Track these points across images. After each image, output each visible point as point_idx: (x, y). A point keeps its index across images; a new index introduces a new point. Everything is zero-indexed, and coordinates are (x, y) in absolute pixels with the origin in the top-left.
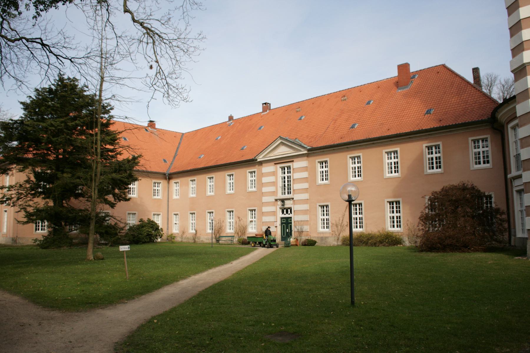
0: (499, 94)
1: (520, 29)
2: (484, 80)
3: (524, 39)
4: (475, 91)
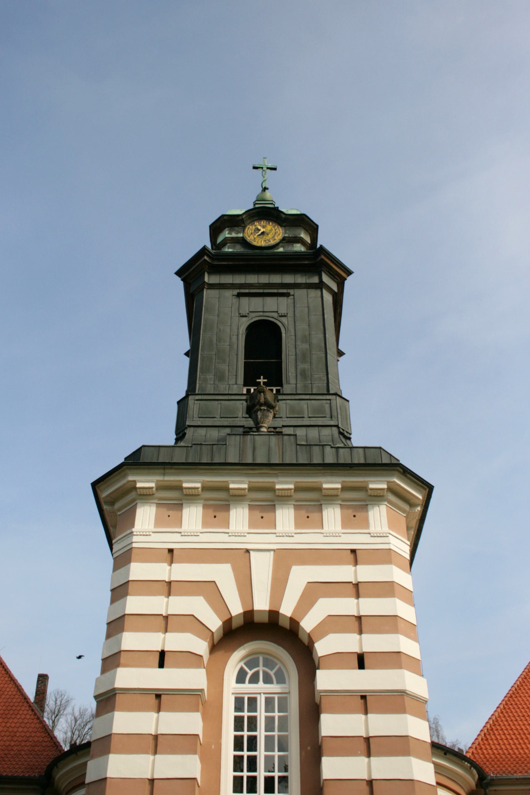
0: (66, 733)
1: (122, 630)
2: (50, 702)
3: (124, 647)
4: (32, 717)
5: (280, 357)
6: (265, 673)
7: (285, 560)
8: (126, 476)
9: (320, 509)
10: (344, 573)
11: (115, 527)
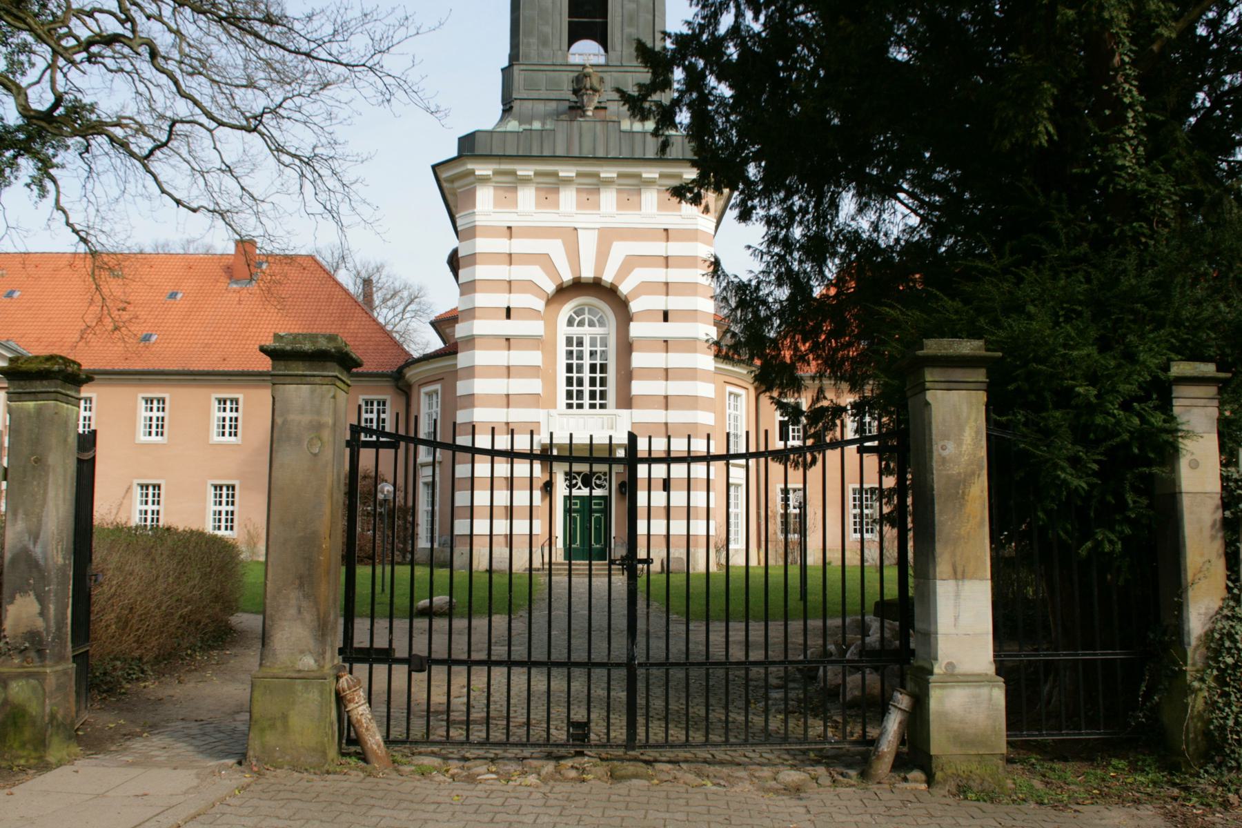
1: (474, 291)
5: (606, 17)
7: (607, 237)
8: (465, 164)
9: (639, 192)
10: (658, 248)
11: (456, 207)
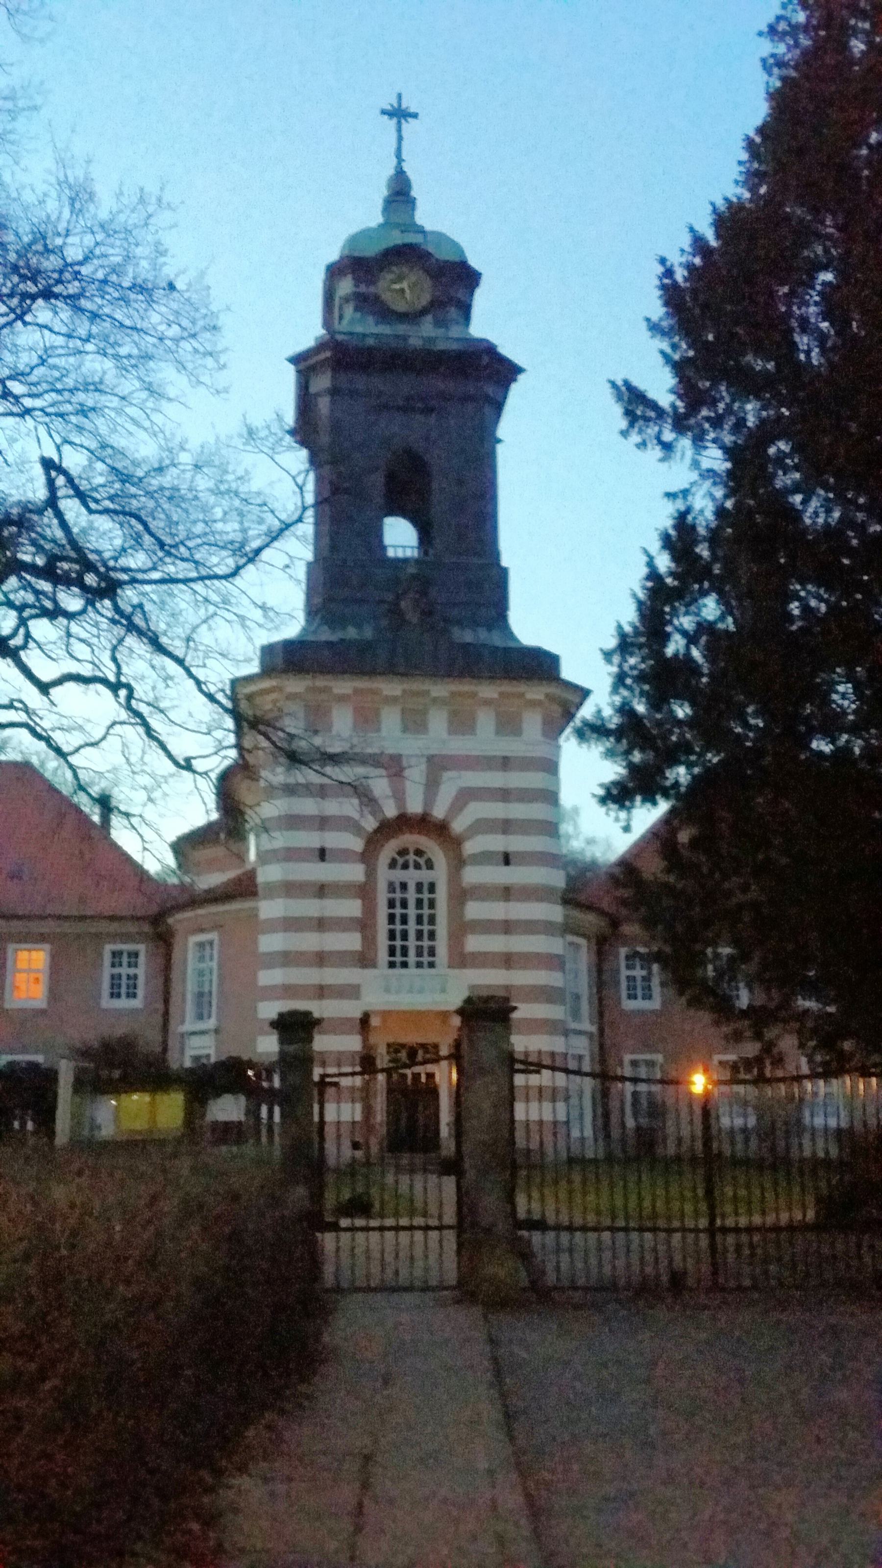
6: (415, 861)
7: (437, 766)
